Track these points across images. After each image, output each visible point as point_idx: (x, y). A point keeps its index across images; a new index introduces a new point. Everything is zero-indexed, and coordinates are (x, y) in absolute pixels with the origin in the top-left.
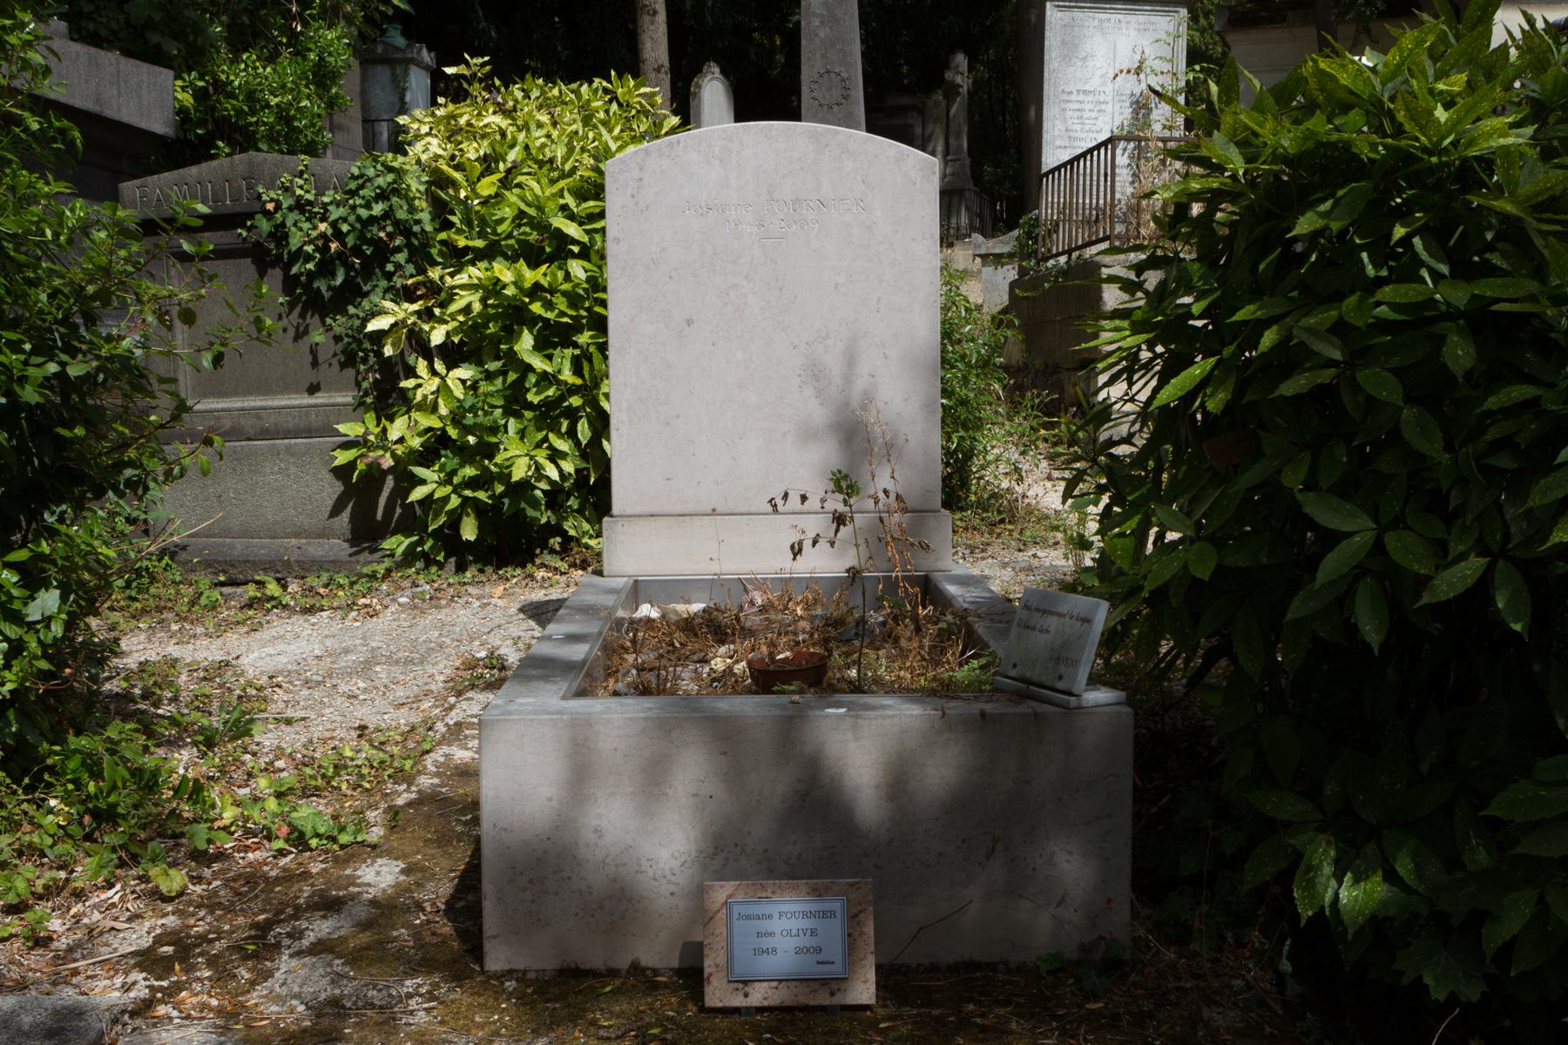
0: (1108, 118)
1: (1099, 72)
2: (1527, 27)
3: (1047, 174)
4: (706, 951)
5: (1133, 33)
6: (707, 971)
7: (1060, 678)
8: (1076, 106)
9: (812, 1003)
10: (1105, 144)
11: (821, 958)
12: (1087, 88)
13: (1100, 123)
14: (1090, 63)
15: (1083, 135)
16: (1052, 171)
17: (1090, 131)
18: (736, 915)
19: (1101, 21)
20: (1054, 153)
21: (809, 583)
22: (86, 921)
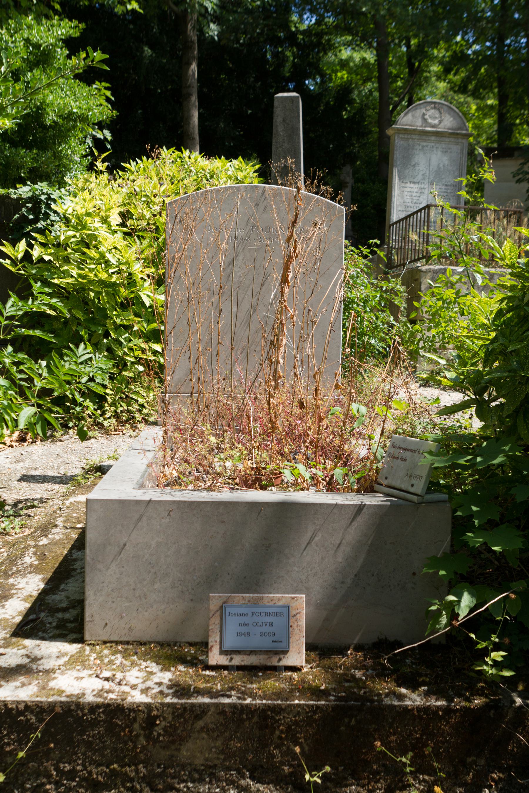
0: (425, 197)
1: (421, 173)
2: (16, 587)
3: (393, 225)
4: (210, 633)
5: (439, 153)
6: (210, 644)
7: (412, 485)
8: (409, 190)
9: (269, 664)
10: (424, 208)
11: (275, 639)
12: (415, 180)
13: (421, 199)
14: (417, 168)
15: (412, 205)
16: (396, 223)
17: (416, 203)
18: (227, 614)
19: (423, 147)
20: (396, 213)
21: (61, 702)
22: (366, 339)
